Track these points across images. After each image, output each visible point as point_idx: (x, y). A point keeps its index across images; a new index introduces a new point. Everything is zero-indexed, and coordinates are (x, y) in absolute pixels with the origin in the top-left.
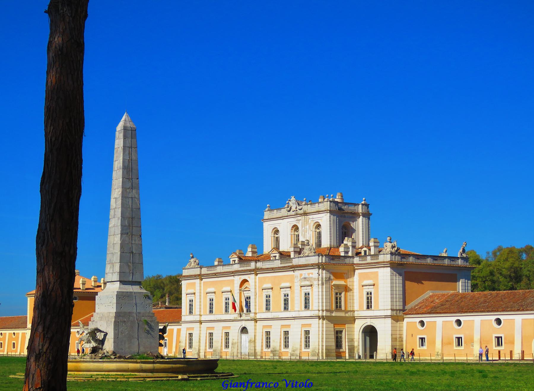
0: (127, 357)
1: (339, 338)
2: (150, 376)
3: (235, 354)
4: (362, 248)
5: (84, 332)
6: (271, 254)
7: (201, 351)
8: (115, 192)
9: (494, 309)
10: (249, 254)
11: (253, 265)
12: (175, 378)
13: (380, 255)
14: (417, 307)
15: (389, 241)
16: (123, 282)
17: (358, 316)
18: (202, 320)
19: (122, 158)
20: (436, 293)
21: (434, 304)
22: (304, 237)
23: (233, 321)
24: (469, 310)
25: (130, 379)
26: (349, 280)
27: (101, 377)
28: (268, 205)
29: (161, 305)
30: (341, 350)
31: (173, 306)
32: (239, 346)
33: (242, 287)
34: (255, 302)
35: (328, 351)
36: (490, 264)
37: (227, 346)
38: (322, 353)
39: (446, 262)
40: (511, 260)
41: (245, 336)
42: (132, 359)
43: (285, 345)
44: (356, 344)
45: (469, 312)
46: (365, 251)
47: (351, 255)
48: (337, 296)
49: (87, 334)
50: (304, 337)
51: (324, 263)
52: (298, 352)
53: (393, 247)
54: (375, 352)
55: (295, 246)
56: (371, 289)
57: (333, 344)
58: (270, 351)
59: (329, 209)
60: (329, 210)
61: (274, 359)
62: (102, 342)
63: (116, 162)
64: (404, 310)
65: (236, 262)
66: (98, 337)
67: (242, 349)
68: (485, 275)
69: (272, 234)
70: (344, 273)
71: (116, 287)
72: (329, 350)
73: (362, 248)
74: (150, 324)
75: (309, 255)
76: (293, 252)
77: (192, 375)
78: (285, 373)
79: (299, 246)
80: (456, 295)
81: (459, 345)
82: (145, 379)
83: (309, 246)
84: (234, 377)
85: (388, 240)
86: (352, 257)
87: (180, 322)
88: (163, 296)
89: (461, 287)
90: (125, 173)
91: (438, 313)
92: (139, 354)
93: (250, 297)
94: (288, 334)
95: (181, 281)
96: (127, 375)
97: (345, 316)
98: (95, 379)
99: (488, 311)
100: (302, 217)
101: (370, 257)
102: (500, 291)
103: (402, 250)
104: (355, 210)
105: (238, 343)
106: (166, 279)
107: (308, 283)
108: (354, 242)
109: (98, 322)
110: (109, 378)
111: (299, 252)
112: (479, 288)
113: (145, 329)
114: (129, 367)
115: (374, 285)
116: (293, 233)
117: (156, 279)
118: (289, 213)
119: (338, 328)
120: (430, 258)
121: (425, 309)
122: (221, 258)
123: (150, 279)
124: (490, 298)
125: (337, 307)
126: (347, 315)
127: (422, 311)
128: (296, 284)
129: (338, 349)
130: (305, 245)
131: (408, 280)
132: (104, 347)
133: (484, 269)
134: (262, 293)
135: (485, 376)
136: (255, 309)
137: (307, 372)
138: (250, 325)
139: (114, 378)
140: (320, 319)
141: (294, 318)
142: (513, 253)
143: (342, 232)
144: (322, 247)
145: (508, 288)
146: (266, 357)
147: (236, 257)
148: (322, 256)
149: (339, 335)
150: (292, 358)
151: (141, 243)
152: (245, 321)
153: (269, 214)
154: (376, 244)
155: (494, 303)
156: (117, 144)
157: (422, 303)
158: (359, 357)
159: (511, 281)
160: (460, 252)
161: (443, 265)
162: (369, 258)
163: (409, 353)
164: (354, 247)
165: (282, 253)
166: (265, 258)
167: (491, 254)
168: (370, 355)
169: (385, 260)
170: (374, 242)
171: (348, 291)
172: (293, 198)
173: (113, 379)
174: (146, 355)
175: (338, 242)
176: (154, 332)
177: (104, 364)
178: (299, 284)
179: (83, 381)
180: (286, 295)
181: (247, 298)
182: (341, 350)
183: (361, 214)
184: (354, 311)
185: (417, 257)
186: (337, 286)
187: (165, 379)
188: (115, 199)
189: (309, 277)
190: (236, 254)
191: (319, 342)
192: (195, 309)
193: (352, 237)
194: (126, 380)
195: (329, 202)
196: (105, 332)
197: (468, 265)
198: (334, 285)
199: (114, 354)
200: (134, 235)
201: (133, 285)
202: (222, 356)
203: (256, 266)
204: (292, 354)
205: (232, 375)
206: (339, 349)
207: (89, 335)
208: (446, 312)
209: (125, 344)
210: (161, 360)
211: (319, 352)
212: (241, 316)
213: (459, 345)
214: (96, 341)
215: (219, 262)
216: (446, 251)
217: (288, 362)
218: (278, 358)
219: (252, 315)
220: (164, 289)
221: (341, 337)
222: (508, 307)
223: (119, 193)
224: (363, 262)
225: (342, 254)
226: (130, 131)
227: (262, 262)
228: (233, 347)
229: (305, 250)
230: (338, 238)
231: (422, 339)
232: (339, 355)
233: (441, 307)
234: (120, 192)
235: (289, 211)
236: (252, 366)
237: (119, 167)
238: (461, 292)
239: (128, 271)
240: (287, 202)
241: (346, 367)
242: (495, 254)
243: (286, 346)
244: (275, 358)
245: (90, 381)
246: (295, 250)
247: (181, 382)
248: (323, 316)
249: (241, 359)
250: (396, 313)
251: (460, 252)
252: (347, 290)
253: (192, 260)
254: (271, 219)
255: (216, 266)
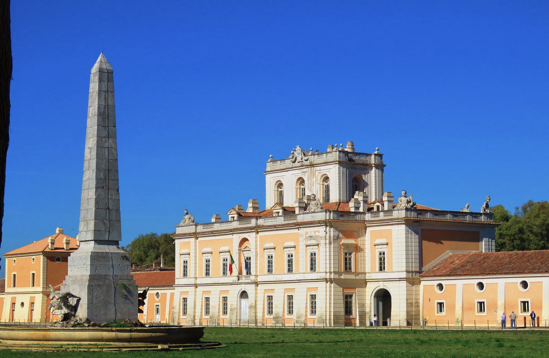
0: (102, 325)
1: (349, 303)
2: (126, 346)
3: (234, 321)
4: (374, 204)
5: (55, 297)
6: (273, 210)
7: (196, 318)
8: (90, 142)
9: (520, 271)
10: (250, 210)
11: (253, 222)
12: (155, 348)
13: (394, 211)
14: (434, 269)
15: (405, 195)
16: (98, 241)
17: (370, 279)
18: (197, 283)
19: (97, 103)
20: (456, 253)
21: (454, 265)
22: (311, 191)
23: (232, 284)
24: (492, 271)
25: (104, 350)
26: (359, 239)
27: (72, 346)
28: (271, 156)
29: (155, 266)
30: (351, 317)
31: (168, 268)
32: (238, 311)
33: (242, 247)
34: (256, 264)
35: (337, 317)
36: (520, 221)
37: (225, 313)
38: (330, 319)
39: (468, 218)
40: (542, 216)
41: (245, 301)
42: (108, 327)
43: (289, 310)
44: (367, 310)
45: (493, 274)
46: (378, 207)
47: (362, 211)
48: (346, 256)
49: (58, 299)
50: (310, 302)
51: (332, 220)
52: (303, 319)
53: (408, 202)
54: (389, 319)
55: (300, 201)
56: (384, 249)
57: (342, 310)
58: (272, 317)
59: (338, 159)
60: (339, 161)
61: (276, 326)
62: (75, 308)
63: (91, 108)
64: (420, 272)
65: (235, 219)
66: (71, 303)
67: (242, 316)
68: (513, 233)
69: (275, 188)
70: (355, 231)
71: (90, 247)
72: (338, 316)
73: (374, 203)
74: (128, 288)
75: (316, 211)
76: (298, 208)
77: (174, 345)
78: (281, 343)
79: (305, 200)
80: (478, 255)
81: (481, 310)
82: (121, 349)
83: (316, 201)
84: (221, 347)
85: (403, 194)
86: (364, 213)
87: (174, 286)
88: (157, 257)
89: (484, 246)
90: (101, 119)
91: (457, 275)
92: (116, 321)
93: (250, 258)
94: (292, 299)
95: (174, 240)
96: (101, 345)
97: (356, 279)
98: (66, 349)
99: (513, 273)
100: (308, 168)
101: (383, 213)
102: (530, 250)
103: (418, 205)
104: (368, 161)
105: (237, 308)
106: (161, 237)
107: (313, 242)
108: (366, 197)
109: (70, 286)
110: (81, 348)
111: (304, 208)
112: (506, 247)
113: (123, 293)
114: (103, 335)
115: (295, 247)
116: (298, 187)
117: (151, 238)
118: (294, 165)
119: (348, 292)
120: (450, 214)
121: (444, 271)
122: (219, 215)
123: (143, 237)
124: (516, 258)
125: (346, 268)
126: (357, 278)
127: (440, 273)
128: (300, 243)
129: (347, 315)
130: (310, 200)
131: (424, 240)
132: (77, 314)
133: (513, 226)
134: (263, 253)
135: (501, 346)
136: (256, 271)
137: (307, 341)
138: (250, 289)
139: (87, 348)
140: (327, 282)
141: (299, 281)
142: (545, 208)
143: (353, 186)
144: (330, 202)
145: (539, 248)
146: (268, 325)
147: (235, 213)
148: (330, 212)
149: (349, 300)
150: (296, 325)
151: (118, 198)
152: (245, 284)
153: (271, 165)
154: (390, 199)
155: (520, 264)
156: (92, 87)
157: (441, 264)
158: (371, 324)
159: (542, 239)
160: (483, 208)
161: (464, 222)
162: (382, 214)
163: (426, 319)
164: (365, 202)
165: (286, 208)
166: (267, 214)
167: (520, 210)
168: (383, 322)
169: (400, 217)
170: (388, 197)
171: (358, 250)
172: (298, 148)
173: (85, 350)
174: (123, 322)
175: (348, 196)
176: (133, 297)
177: (76, 332)
178: (304, 243)
179: (52, 351)
180: (289, 255)
181: (247, 258)
182: (351, 316)
183: (373, 165)
184: (365, 273)
185: (435, 213)
186: (346, 246)
187: (143, 349)
188: (89, 149)
189: (316, 236)
190: (235, 209)
191: (326, 307)
192: (190, 271)
193: (364, 191)
194: (100, 350)
195: (338, 152)
196: (78, 297)
197: (492, 222)
198: (343, 244)
199: (88, 322)
200: (110, 189)
201: (110, 245)
202: (220, 323)
203: (256, 223)
204: (296, 321)
205: (220, 344)
206: (349, 315)
207: (61, 301)
208: (467, 274)
209: (100, 310)
210: (139, 328)
211: (326, 319)
212: (239, 280)
213: (481, 310)
214: (68, 307)
215: (216, 219)
216: (468, 206)
217: (292, 330)
218: (281, 325)
219: (252, 278)
220: (158, 249)
221: (351, 302)
222: (535, 269)
223: (94, 143)
224: (376, 218)
225: (353, 210)
226: (106, 74)
227: (263, 219)
228: (232, 313)
229: (311, 205)
230: (348, 192)
231: (441, 305)
232: (348, 322)
233: (461, 269)
234: (94, 141)
235: (294, 162)
236: (248, 335)
237: (94, 113)
238: (484, 252)
239: (103, 229)
240: (292, 152)
241: (352, 336)
242: (524, 209)
243: (290, 312)
244: (277, 325)
245: (60, 351)
246: (300, 206)
247: (161, 353)
248: (330, 279)
249: (239, 327)
250: (412, 276)
251: (483, 208)
252: (357, 250)
253: (187, 217)
254: (274, 171)
255: (213, 223)
